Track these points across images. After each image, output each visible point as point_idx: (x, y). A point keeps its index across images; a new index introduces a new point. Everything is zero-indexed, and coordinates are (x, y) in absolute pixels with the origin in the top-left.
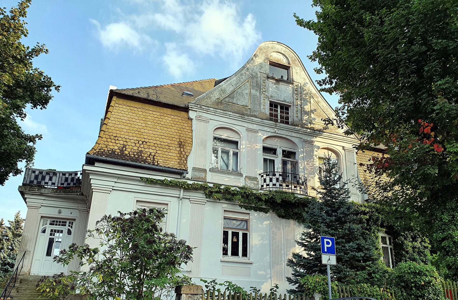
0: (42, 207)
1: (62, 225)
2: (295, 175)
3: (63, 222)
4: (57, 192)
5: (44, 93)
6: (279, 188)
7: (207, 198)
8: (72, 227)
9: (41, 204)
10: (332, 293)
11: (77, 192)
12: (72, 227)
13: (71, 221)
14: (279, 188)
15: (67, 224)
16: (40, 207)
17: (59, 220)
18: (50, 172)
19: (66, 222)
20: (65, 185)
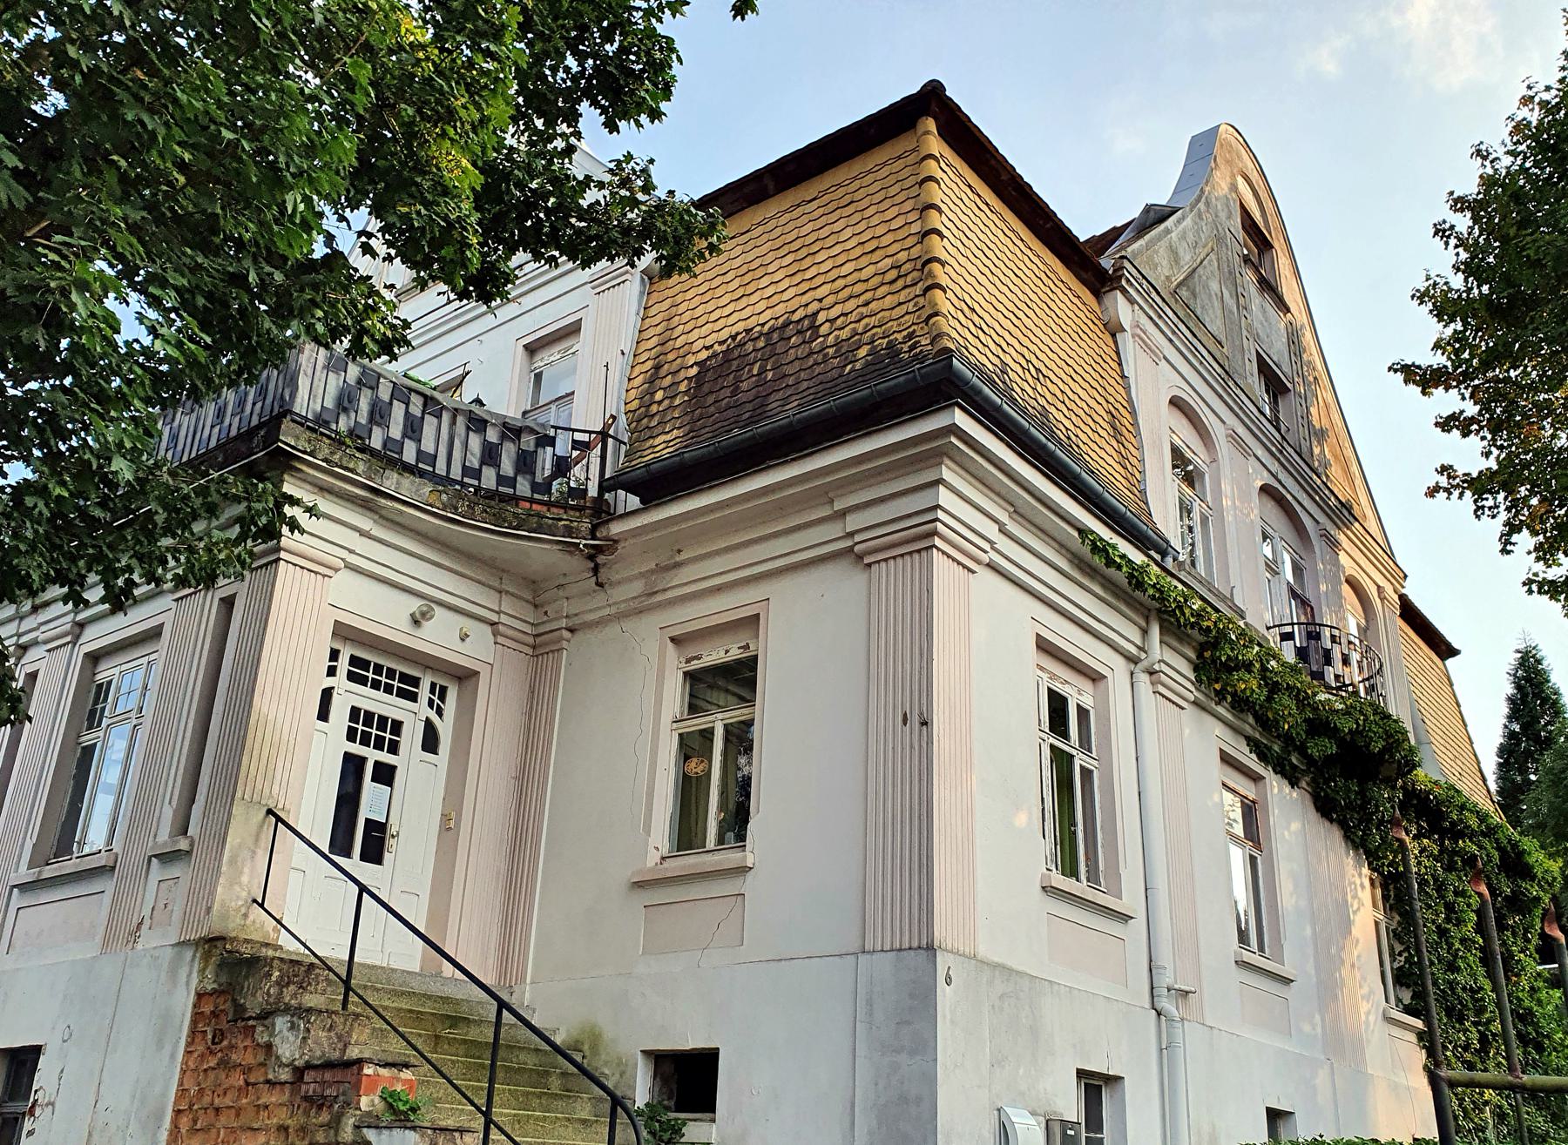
0: (344, 575)
1: (402, 694)
2: (1311, 628)
3: (404, 678)
4: (455, 510)
5: (1304, 784)
6: (532, 501)
7: (585, 264)
8: (440, 712)
9: (344, 554)
10: (1511, 1002)
11: (569, 531)
12: (440, 712)
13: (440, 682)
14: (532, 501)
15: (424, 692)
16: (337, 570)
17: (387, 663)
18: (411, 390)
19: (415, 682)
20: (489, 479)
